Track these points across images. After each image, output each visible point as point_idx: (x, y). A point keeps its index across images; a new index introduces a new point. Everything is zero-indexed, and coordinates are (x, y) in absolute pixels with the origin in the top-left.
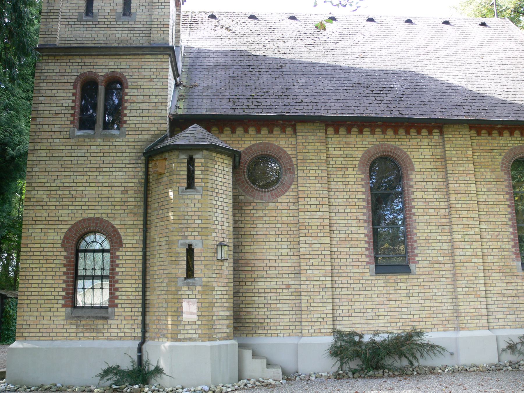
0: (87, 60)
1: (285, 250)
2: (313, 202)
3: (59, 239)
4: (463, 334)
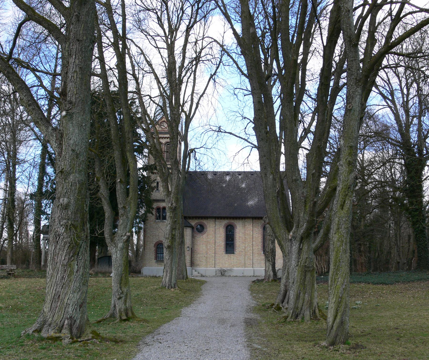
0: (158, 203)
1: (204, 248)
2: (211, 236)
3: (153, 245)
4: (246, 268)
